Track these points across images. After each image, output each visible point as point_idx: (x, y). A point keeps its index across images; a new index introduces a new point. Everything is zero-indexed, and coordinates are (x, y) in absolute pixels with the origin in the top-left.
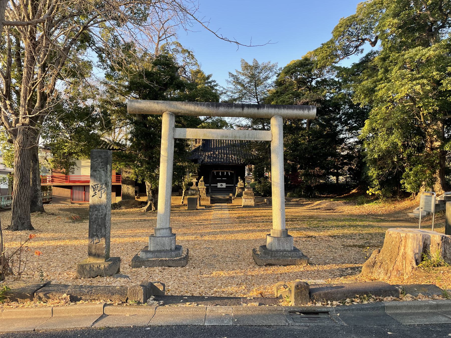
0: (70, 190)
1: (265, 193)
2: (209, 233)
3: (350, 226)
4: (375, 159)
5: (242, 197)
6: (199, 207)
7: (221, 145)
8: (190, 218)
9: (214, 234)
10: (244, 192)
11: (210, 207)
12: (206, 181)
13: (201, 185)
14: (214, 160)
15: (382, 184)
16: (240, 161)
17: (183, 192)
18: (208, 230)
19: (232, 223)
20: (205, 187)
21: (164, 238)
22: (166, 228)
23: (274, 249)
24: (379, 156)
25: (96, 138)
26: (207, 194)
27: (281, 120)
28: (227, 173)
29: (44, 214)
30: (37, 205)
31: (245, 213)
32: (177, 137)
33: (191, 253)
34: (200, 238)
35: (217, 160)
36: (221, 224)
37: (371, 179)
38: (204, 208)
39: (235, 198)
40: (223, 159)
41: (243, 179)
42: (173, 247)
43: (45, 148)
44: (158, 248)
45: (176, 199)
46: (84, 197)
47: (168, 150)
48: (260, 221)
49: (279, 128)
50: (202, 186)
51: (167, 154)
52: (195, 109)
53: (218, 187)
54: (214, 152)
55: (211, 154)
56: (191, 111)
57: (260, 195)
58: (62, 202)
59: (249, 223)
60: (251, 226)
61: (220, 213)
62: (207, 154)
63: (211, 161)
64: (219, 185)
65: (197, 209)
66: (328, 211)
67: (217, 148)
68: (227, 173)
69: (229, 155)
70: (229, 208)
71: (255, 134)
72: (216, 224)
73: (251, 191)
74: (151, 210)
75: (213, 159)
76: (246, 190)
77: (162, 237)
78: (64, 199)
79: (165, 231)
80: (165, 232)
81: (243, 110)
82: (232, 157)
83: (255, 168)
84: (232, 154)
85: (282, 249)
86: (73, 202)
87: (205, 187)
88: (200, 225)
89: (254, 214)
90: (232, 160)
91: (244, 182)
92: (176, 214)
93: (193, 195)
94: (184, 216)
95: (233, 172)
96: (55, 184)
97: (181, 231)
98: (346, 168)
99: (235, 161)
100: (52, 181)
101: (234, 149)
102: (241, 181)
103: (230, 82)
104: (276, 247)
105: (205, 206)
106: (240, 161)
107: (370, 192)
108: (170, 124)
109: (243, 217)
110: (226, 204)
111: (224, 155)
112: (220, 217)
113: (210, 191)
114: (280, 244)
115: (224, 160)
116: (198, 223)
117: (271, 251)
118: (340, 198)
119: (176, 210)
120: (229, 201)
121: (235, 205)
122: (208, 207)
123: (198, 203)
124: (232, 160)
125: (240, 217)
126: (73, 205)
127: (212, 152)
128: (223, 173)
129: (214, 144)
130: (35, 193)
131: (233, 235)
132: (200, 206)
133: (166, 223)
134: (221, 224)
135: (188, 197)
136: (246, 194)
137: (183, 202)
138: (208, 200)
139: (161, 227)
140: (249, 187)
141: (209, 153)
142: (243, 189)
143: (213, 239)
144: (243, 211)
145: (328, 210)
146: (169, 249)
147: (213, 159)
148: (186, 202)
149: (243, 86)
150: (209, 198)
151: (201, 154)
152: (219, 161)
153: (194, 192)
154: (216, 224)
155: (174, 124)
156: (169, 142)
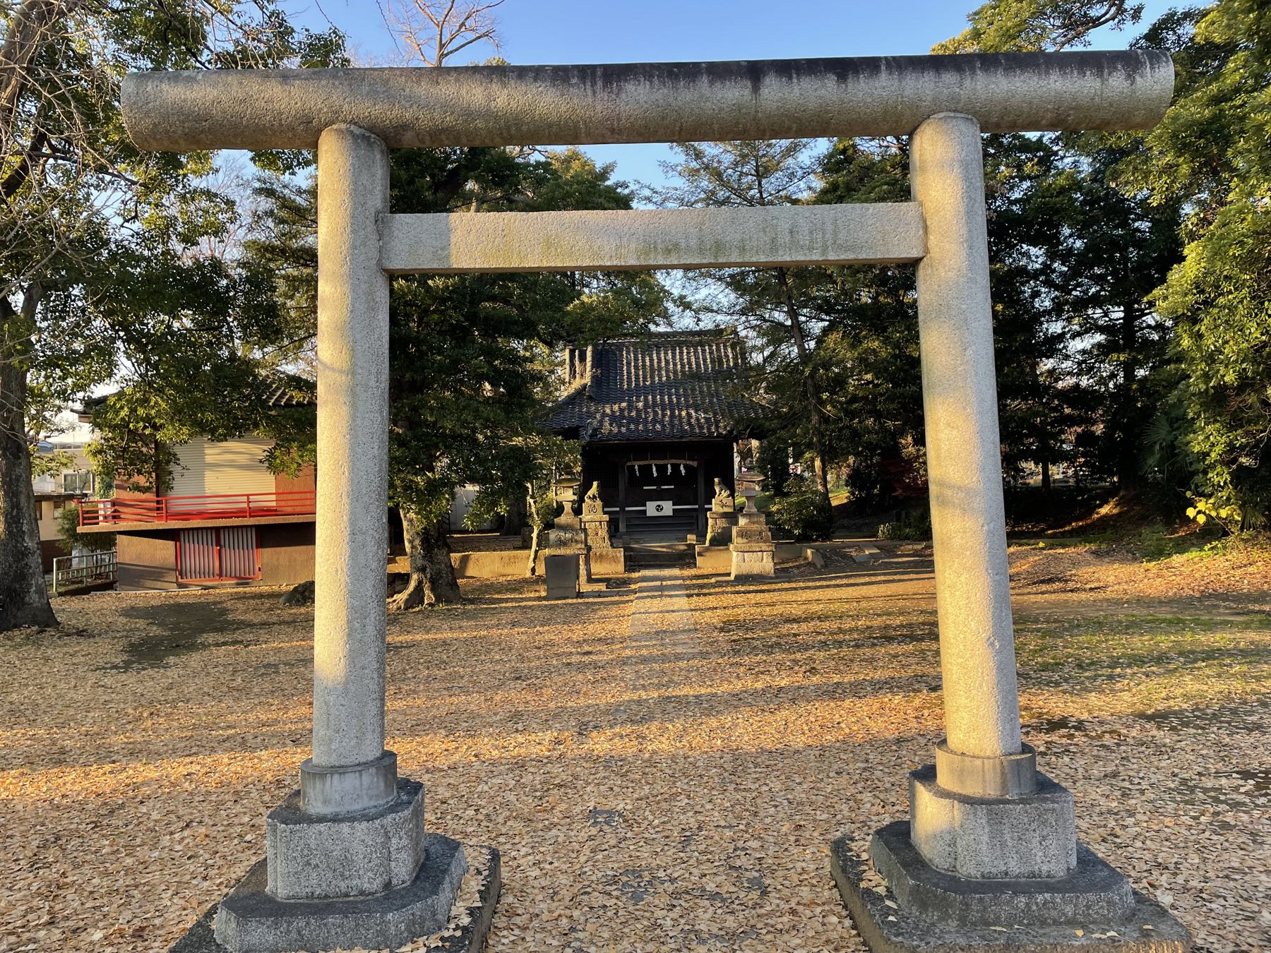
0: (172, 543)
1: (804, 528)
2: (614, 714)
3: (1191, 657)
4: (1222, 389)
5: (731, 546)
6: (585, 587)
7: (652, 377)
8: (550, 633)
9: (638, 715)
10: (734, 530)
11: (625, 582)
12: (607, 498)
13: (592, 510)
14: (632, 426)
15: (1240, 477)
16: (717, 427)
17: (534, 535)
18: (609, 695)
19: (704, 655)
20: (606, 517)
21: (345, 828)
22: (362, 766)
23: (968, 869)
24: (1242, 375)
25: (239, 372)
26: (611, 538)
27: (975, 136)
28: (676, 468)
29: (51, 631)
30: (24, 604)
31: (746, 605)
32: (399, 263)
33: (522, 862)
34: (572, 749)
35: (641, 427)
36: (664, 658)
37: (1201, 466)
38: (602, 587)
39: (707, 550)
40: (662, 422)
41: (729, 484)
42: (402, 870)
43: (84, 413)
44: (316, 883)
45: (513, 561)
46: (217, 564)
47: (352, 331)
48: (810, 640)
49: (967, 179)
50: (594, 515)
51: (345, 356)
52: (491, 98)
53: (648, 514)
54: (630, 402)
55: (621, 410)
56: (469, 114)
57: (788, 534)
58: (149, 583)
59: (770, 649)
60: (780, 666)
61: (658, 609)
62: (608, 411)
63: (623, 430)
64: (651, 508)
65: (580, 595)
66: (1044, 587)
67: (640, 391)
68: (676, 468)
69: (680, 410)
70: (687, 587)
71: (829, 227)
72: (644, 660)
73: (761, 525)
74: (422, 602)
75: (629, 423)
76: (742, 521)
77: (336, 819)
78: (151, 574)
79: (350, 781)
80: (358, 791)
81: (756, 89)
82: (689, 415)
83: (762, 449)
84: (687, 407)
85: (1015, 867)
86: (184, 581)
87: (606, 517)
88: (581, 667)
89: (779, 609)
90: (689, 424)
91: (732, 495)
92: (506, 618)
93: (562, 543)
94: (531, 623)
95: (695, 464)
96: (123, 526)
97: (506, 701)
98: (1070, 435)
99: (701, 427)
100: (116, 517)
101: (693, 390)
102: (725, 493)
103: (673, 168)
104: (979, 856)
105: (607, 581)
106: (717, 427)
107: (1200, 511)
108: (358, 193)
109: (742, 625)
110: (676, 572)
111: (663, 410)
112: (659, 627)
113: (622, 528)
114: (1003, 845)
115: (663, 426)
116: (574, 659)
117: (954, 883)
118: (1072, 533)
119: (507, 600)
120: (686, 559)
121: (706, 572)
122: (616, 585)
123: (582, 571)
124: (689, 424)
125: (729, 622)
126: (182, 592)
127: (624, 404)
128: (662, 469)
129: (629, 378)
130: (17, 561)
131: (714, 723)
132: (590, 580)
133: (360, 739)
134: (664, 658)
135: (547, 552)
136: (742, 534)
137: (533, 570)
138: (615, 559)
139: (333, 760)
140: (754, 510)
141: (616, 407)
142: (732, 517)
143: (631, 748)
144: (740, 599)
145: (1043, 582)
146: (377, 885)
147: (629, 423)
148: (541, 570)
149: (719, 175)
150: (620, 553)
151: (588, 412)
152: (646, 430)
153: (569, 535)
154: (644, 660)
155: (378, 194)
156: (354, 289)
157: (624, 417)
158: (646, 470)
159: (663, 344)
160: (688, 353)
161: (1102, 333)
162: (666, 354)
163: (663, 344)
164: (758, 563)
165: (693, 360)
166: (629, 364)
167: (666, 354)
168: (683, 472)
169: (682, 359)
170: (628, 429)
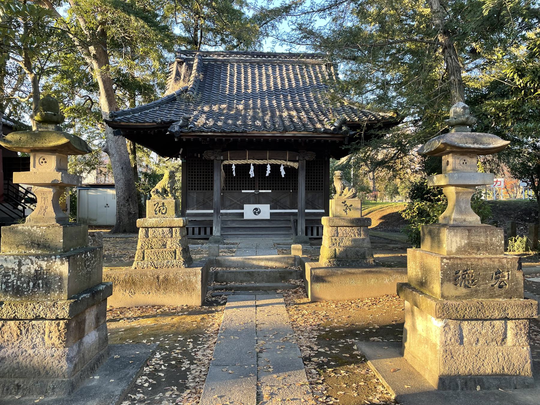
53: (246, 217)
68: (275, 168)
75: (227, 119)
87: (180, 222)
95: (296, 165)
127: (224, 106)
129: (231, 86)
138: (187, 287)
147: (227, 119)
157: (222, 114)
158: (243, 169)
159: (264, 62)
160: (287, 70)
161: (100, 290)
162: (267, 70)
163: (264, 62)
164: (494, 348)
165: (292, 76)
166: (232, 75)
167: (267, 70)
168: (283, 173)
169: (281, 74)
170: (225, 123)
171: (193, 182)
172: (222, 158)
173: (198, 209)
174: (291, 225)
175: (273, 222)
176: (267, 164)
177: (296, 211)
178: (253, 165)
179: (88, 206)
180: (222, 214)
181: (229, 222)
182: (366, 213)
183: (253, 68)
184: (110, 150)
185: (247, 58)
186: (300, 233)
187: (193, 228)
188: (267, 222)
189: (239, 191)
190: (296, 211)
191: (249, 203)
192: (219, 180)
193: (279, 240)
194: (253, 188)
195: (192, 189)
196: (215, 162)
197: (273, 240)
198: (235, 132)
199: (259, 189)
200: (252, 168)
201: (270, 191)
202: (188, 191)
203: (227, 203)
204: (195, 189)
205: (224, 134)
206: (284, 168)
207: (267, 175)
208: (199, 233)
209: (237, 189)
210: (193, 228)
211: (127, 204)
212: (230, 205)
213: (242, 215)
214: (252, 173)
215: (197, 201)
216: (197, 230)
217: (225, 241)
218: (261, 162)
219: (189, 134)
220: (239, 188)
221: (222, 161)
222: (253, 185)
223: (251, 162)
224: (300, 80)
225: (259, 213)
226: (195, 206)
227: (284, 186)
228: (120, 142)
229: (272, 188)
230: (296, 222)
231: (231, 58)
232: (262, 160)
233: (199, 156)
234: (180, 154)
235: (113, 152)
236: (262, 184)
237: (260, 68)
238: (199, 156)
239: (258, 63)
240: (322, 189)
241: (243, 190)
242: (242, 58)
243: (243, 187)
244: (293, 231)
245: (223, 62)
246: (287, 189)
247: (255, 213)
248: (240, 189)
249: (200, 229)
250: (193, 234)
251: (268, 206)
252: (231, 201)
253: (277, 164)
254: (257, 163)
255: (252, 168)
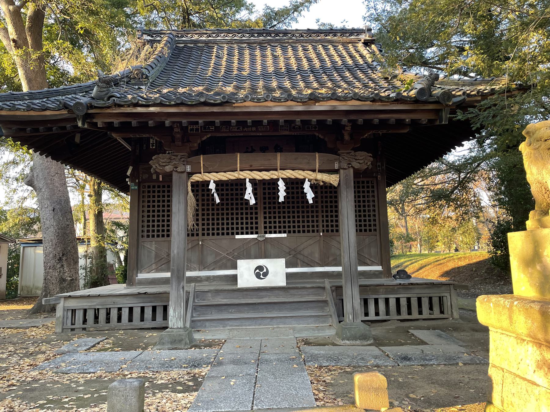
53: (242, 283)
68: (295, 186)
95: (333, 179)
159: (269, 42)
163: (269, 42)
168: (310, 196)
171: (151, 224)
172: (189, 169)
173: (158, 270)
174: (327, 296)
175: (292, 291)
176: (278, 180)
177: (340, 269)
178: (250, 181)
179: (34, 273)
180: (191, 280)
181: (210, 295)
182: (416, 268)
183: (252, 49)
184: (36, 183)
185: (244, 38)
186: (349, 317)
187: (143, 309)
188: (281, 293)
189: (230, 236)
190: (340, 269)
191: (248, 256)
192: (182, 211)
193: (307, 329)
194: (254, 230)
195: (148, 236)
196: (175, 176)
197: (294, 329)
198: (205, 104)
199: (266, 233)
200: (249, 188)
201: (284, 235)
202: (141, 240)
203: (210, 259)
204: (153, 236)
205: (184, 110)
206: (311, 187)
207: (281, 199)
208: (154, 318)
209: (228, 234)
210: (143, 309)
211: (59, 266)
212: (215, 263)
213: (234, 278)
214: (249, 195)
215: (157, 256)
216: (148, 313)
217: (197, 336)
218: (266, 175)
219: (109, 111)
220: (230, 231)
221: (190, 174)
222: (254, 226)
223: (247, 175)
224: (327, 59)
225: (266, 274)
226: (154, 266)
227: (308, 226)
228: (53, 170)
229: (287, 229)
230: (338, 290)
231: (219, 38)
232: (268, 170)
233: (161, 179)
234: (128, 177)
235: (41, 185)
236: (270, 218)
237: (263, 49)
238: (161, 179)
239: (260, 43)
240: (375, 230)
241: (238, 234)
242: (236, 38)
243: (237, 228)
244: (331, 309)
245: (206, 43)
246: (313, 231)
247: (258, 276)
248: (233, 234)
249: (154, 309)
250: (142, 320)
251: (282, 261)
252: (217, 254)
253: (297, 179)
254: (258, 178)
255: (249, 188)
